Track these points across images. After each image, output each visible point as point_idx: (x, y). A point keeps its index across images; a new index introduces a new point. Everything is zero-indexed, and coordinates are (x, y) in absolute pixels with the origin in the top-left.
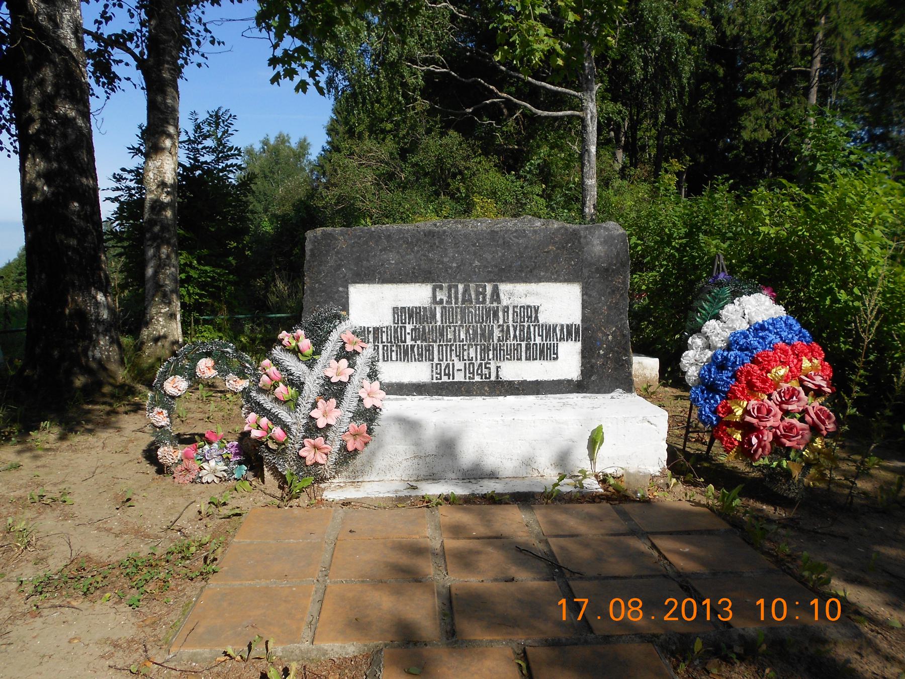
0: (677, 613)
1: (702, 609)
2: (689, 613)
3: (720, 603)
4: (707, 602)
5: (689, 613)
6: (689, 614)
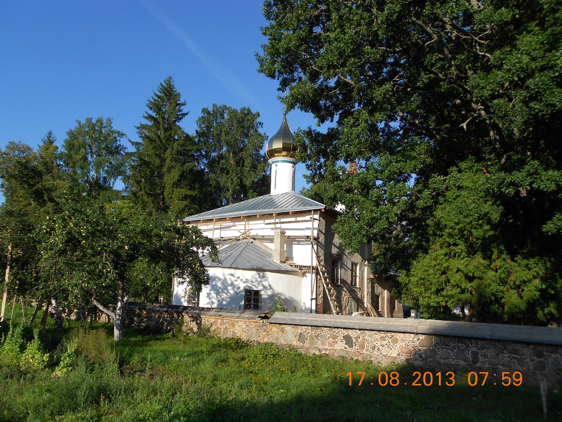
0: (421, 381)
1: (435, 378)
2: (428, 381)
3: (447, 374)
4: (439, 374)
5: (428, 381)
6: (428, 382)
